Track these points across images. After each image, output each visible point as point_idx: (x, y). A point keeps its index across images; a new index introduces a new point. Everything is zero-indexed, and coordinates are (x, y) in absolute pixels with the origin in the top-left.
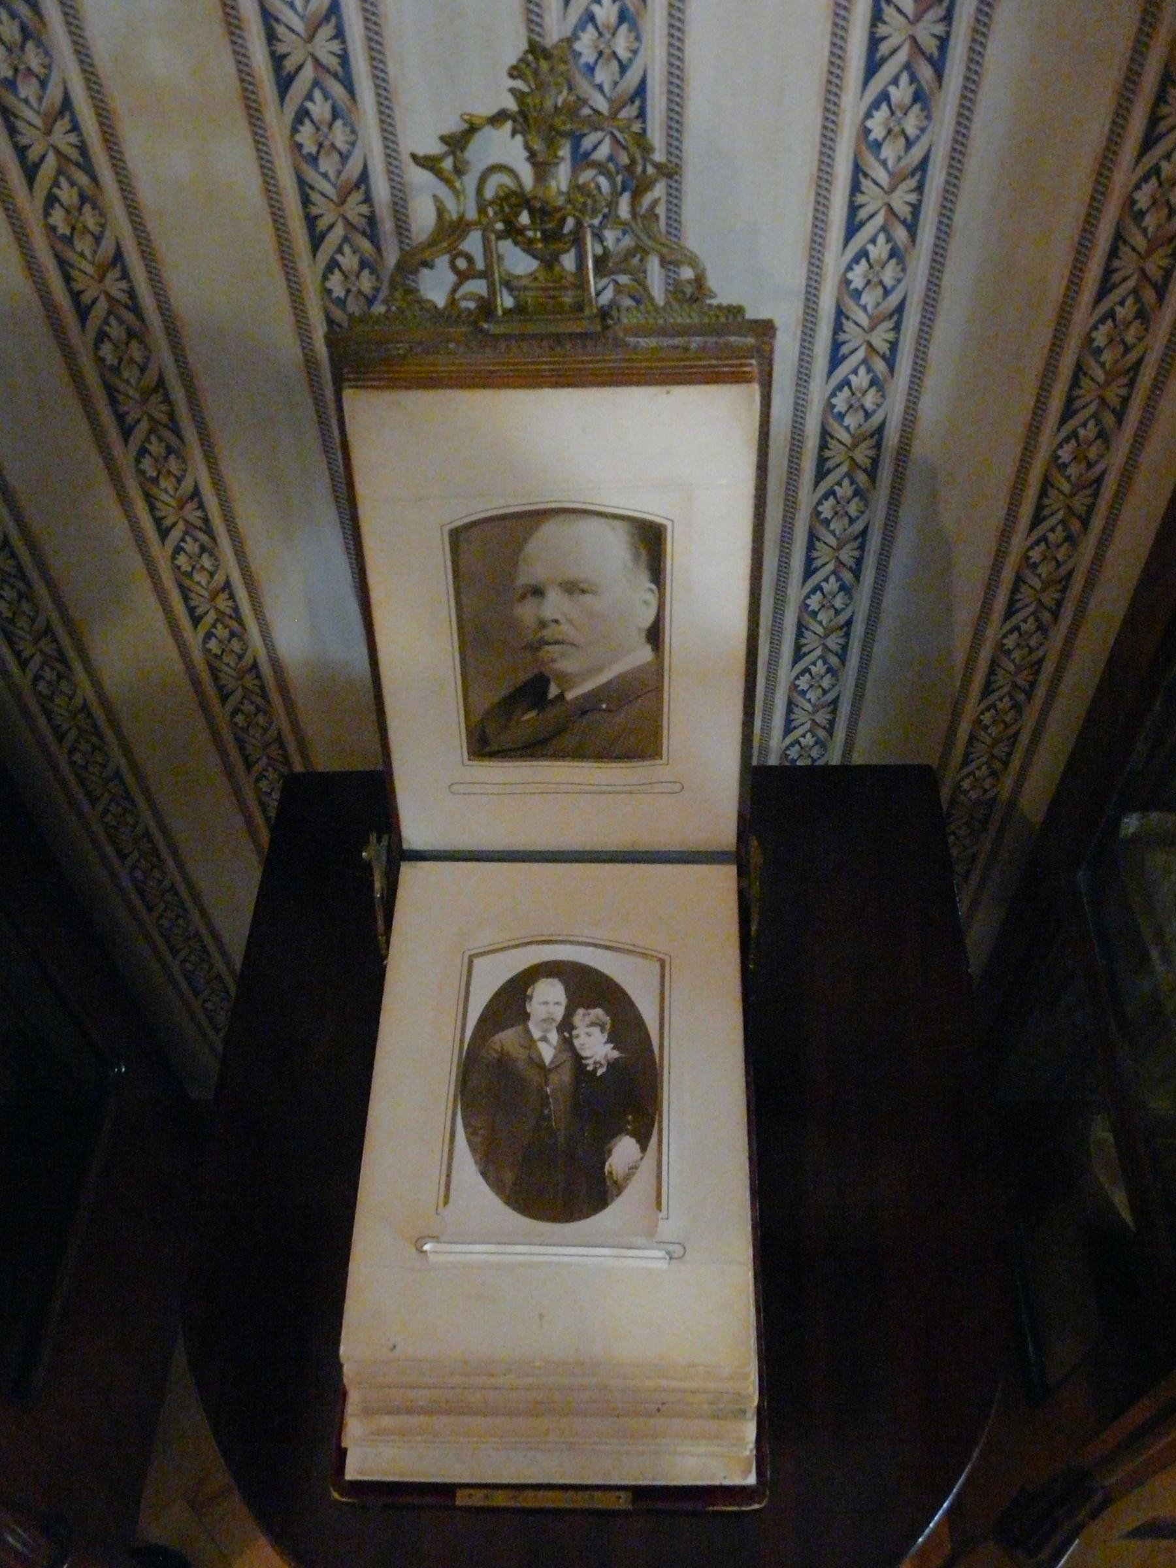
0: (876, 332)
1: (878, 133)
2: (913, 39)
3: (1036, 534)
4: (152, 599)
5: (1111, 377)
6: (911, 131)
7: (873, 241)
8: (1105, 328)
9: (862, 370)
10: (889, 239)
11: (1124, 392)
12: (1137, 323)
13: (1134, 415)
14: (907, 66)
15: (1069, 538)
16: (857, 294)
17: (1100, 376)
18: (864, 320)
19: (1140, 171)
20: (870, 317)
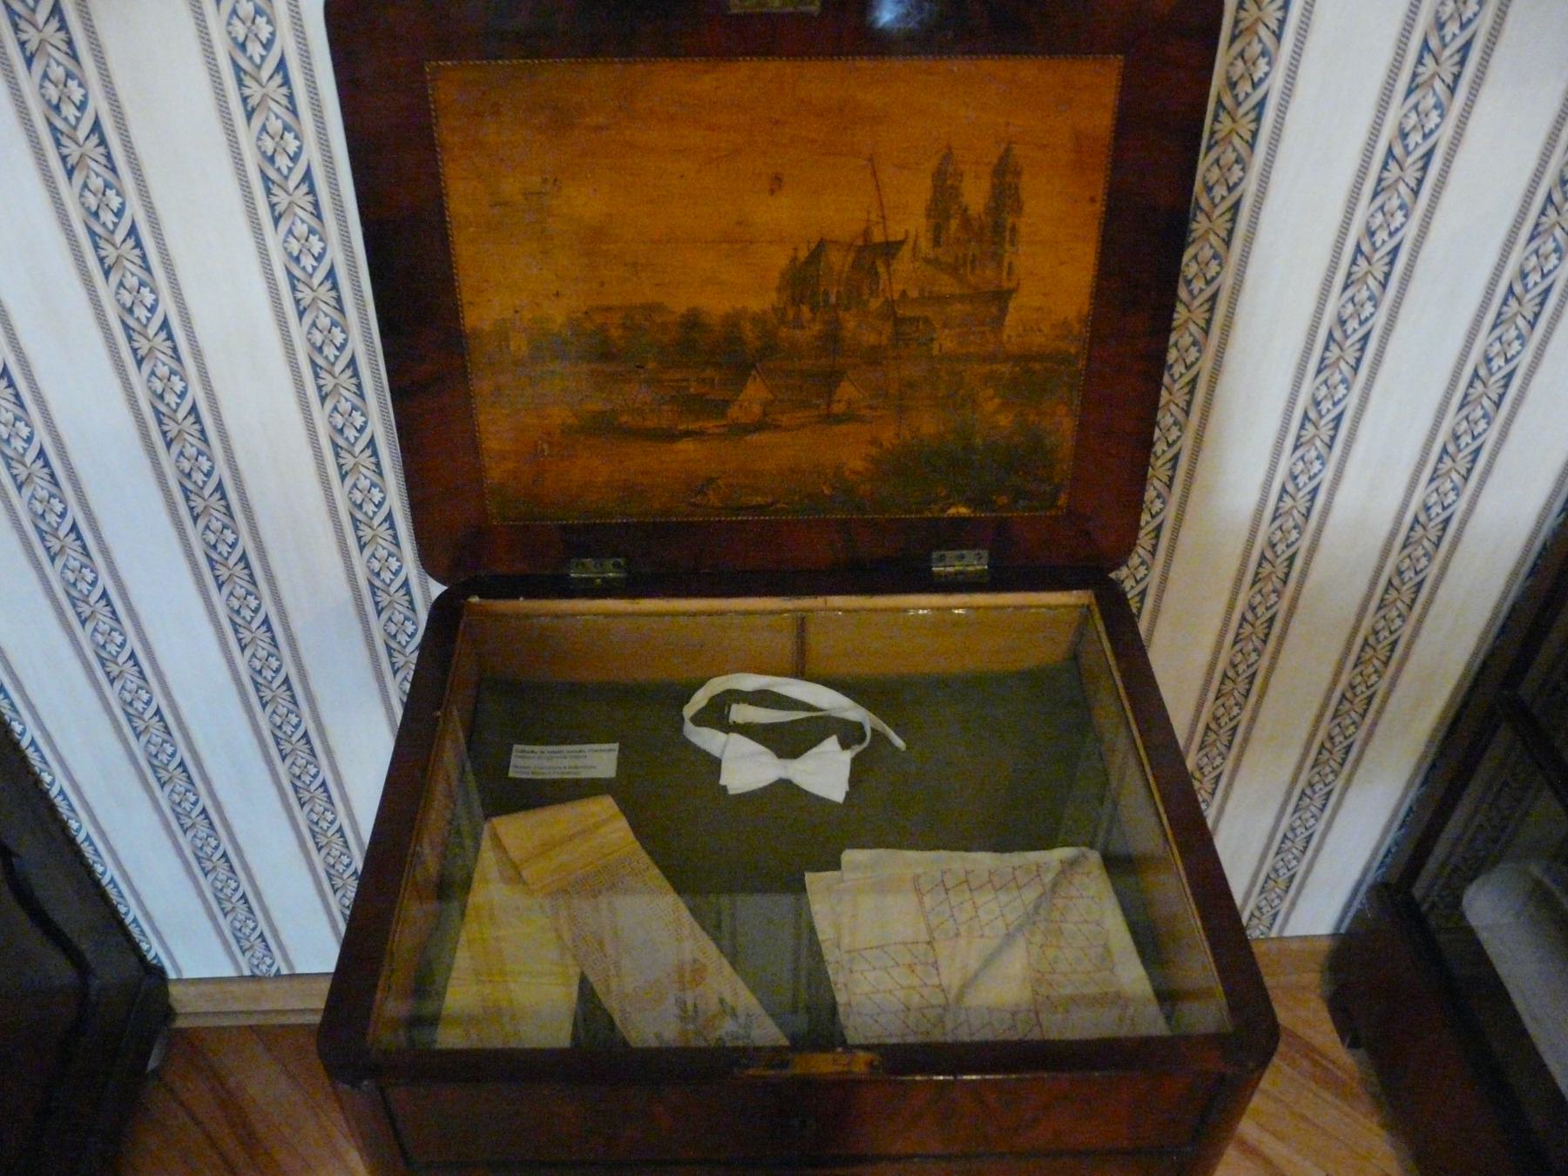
0: (1226, 130)
1: (1237, 168)
2: (1234, 121)
3: (1292, 550)
4: (1137, 776)
5: (1429, 83)
6: (1240, 63)
7: (1223, 198)
8: (1430, 125)
9: (1196, 292)
10: (1212, 199)
11: (1328, 354)
12: (1407, 129)
13: (1218, 676)
14: (1239, 104)
15: (1317, 404)
16: (1195, 343)
17: (1342, 365)
18: (1212, 238)
19: (1370, 323)
20: (1256, 33)
